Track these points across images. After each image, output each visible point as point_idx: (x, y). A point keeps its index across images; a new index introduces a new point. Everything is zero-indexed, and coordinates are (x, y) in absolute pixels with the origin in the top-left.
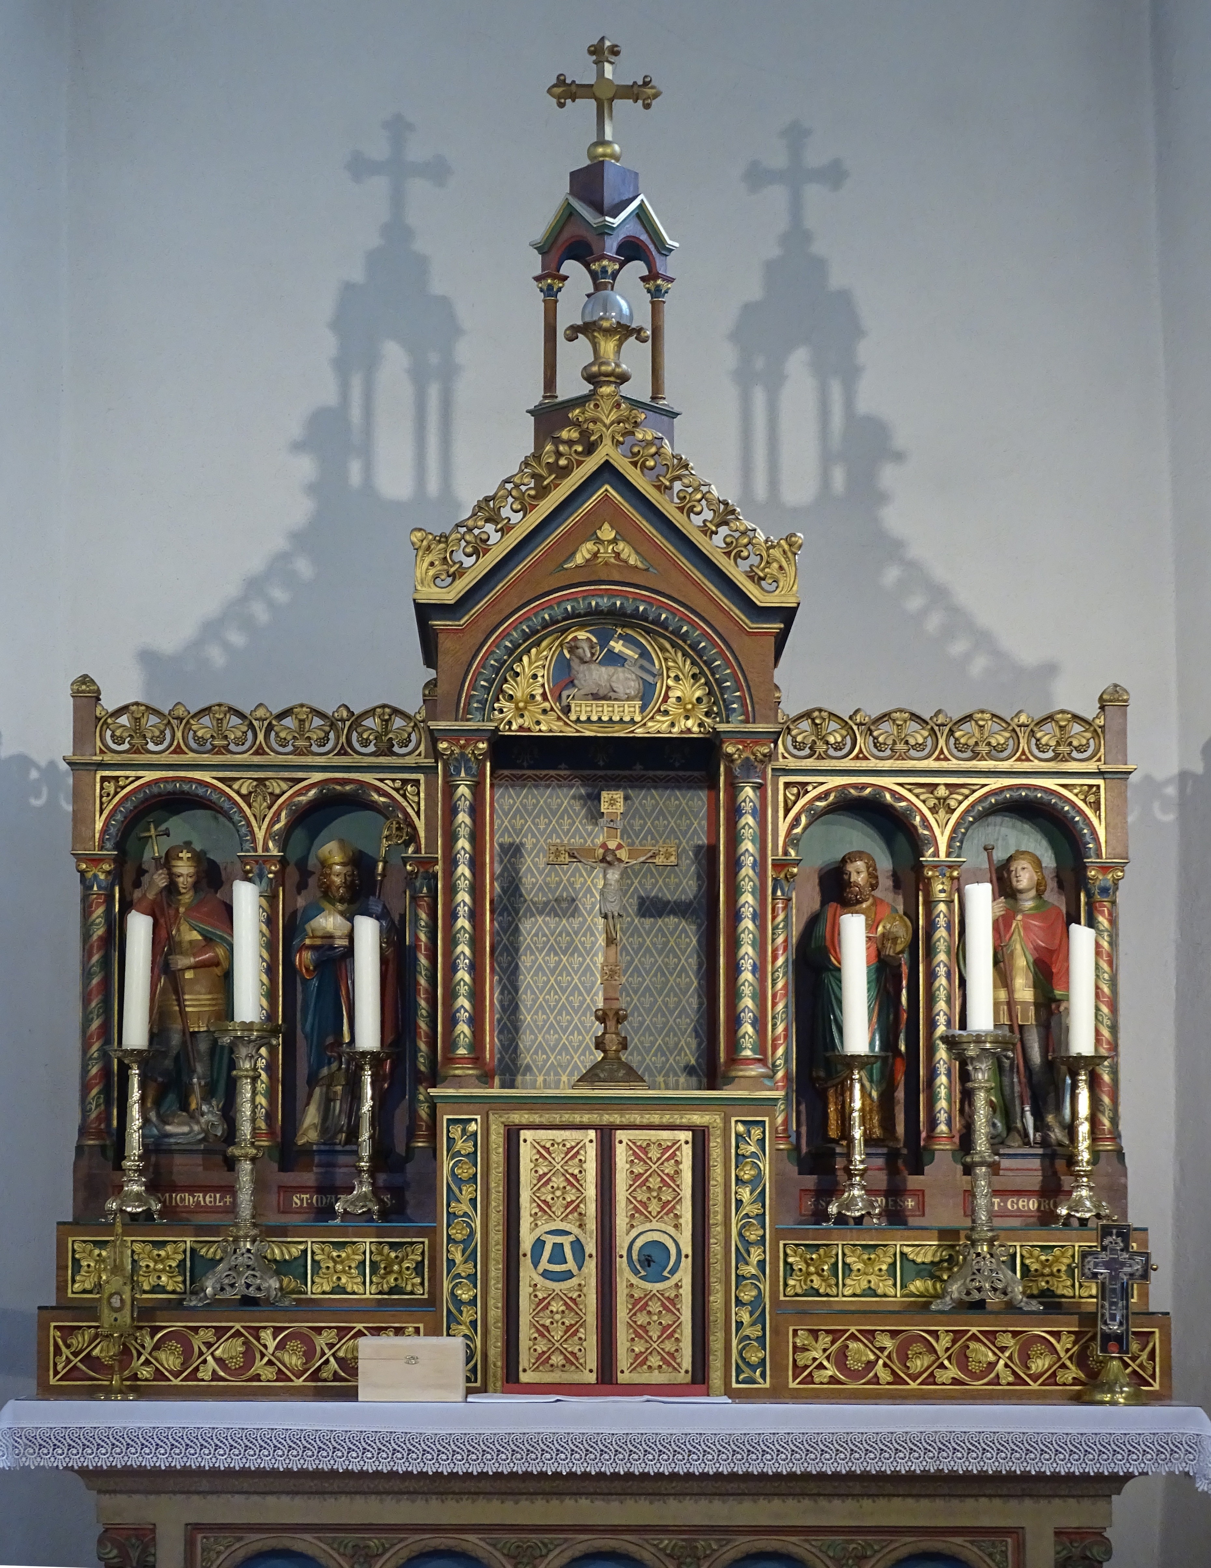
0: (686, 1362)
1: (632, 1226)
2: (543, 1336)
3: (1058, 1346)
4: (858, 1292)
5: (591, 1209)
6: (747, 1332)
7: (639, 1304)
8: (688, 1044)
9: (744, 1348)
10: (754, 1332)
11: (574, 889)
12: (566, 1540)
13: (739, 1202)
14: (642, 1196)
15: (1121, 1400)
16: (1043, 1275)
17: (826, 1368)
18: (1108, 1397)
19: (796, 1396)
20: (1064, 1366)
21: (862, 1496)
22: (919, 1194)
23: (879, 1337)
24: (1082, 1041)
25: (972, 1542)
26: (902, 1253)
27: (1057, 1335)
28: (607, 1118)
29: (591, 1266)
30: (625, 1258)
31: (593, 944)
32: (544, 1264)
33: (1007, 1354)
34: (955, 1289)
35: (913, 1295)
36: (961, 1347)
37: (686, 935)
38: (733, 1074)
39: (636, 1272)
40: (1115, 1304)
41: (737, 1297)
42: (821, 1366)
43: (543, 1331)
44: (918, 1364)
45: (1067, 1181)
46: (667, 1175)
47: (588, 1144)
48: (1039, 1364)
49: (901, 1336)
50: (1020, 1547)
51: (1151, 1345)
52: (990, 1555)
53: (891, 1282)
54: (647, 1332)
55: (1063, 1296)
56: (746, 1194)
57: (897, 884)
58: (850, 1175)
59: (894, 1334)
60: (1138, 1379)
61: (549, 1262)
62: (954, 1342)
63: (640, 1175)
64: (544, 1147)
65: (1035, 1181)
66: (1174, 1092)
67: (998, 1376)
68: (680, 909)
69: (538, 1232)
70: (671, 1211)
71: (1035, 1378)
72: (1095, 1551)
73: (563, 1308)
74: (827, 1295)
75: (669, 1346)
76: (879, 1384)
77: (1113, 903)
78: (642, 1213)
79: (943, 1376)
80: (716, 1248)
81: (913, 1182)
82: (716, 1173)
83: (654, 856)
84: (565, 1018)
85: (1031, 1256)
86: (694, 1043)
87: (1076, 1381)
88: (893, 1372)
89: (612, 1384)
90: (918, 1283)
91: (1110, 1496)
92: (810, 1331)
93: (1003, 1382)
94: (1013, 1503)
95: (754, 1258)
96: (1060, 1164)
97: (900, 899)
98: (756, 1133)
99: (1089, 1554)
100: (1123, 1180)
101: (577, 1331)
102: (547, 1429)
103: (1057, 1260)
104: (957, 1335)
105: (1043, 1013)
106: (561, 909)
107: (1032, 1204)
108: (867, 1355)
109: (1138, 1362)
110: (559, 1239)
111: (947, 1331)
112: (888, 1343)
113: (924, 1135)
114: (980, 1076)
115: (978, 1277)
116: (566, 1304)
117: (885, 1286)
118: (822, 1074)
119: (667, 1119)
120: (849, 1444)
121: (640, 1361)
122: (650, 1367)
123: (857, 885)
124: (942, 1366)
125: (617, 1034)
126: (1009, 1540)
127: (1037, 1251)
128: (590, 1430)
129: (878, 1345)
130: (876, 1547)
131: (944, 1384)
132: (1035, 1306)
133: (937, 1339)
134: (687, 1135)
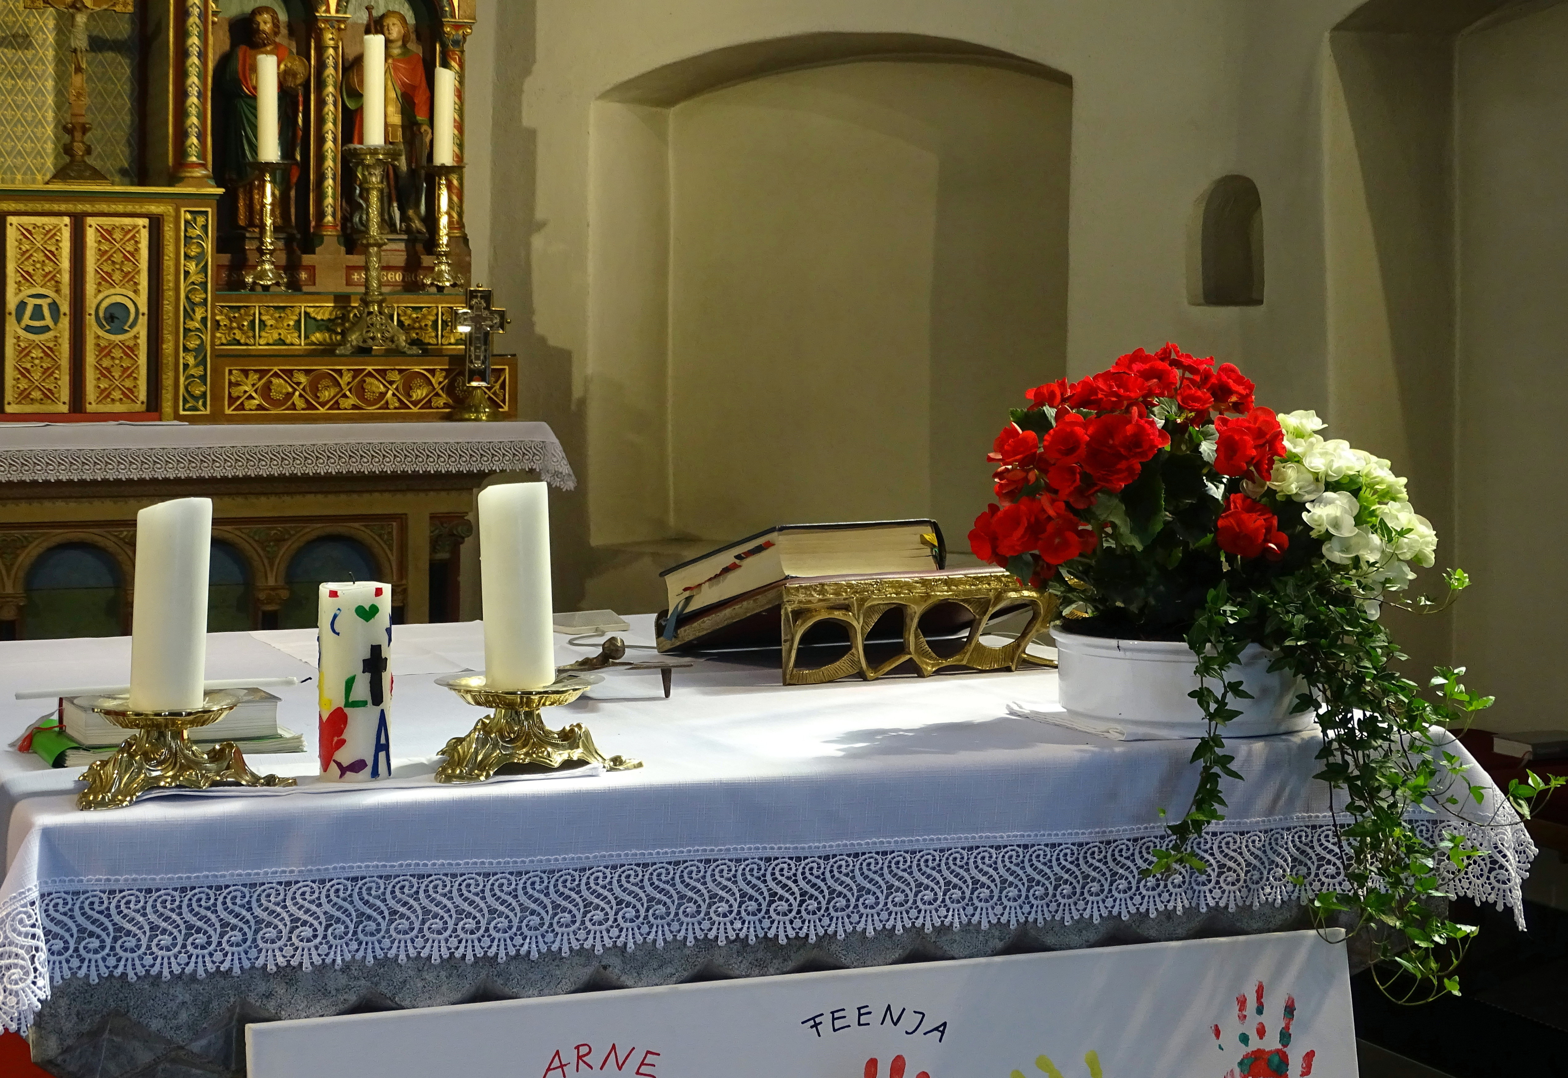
0: (142, 395)
1: (100, 291)
2: (26, 377)
3: (433, 381)
4: (271, 341)
5: (65, 278)
6: (192, 372)
7: (104, 351)
8: (122, 152)
9: (189, 384)
10: (198, 372)
11: (28, 28)
12: (43, 534)
13: (187, 273)
14: (107, 268)
16: (414, 328)
17: (253, 398)
19: (231, 420)
20: (437, 394)
21: (283, 493)
22: (311, 270)
23: (296, 375)
24: (444, 155)
25: (365, 526)
26: (306, 313)
27: (432, 372)
28: (80, 207)
29: (65, 323)
30: (93, 317)
31: (44, 71)
32: (26, 320)
34: (354, 338)
35: (314, 344)
36: (359, 382)
37: (121, 68)
38: (183, 175)
39: (102, 326)
40: (479, 348)
41: (184, 345)
42: (251, 397)
43: (24, 373)
44: (326, 395)
45: (427, 260)
46: (128, 252)
47: (63, 228)
48: (419, 393)
50: (403, 529)
52: (380, 536)
53: (296, 335)
54: (110, 372)
55: (429, 344)
56: (192, 267)
57: (292, 32)
58: (262, 253)
59: (307, 372)
60: (494, 405)
61: (31, 319)
62: (354, 378)
63: (106, 252)
64: (27, 230)
65: (400, 259)
66: (489, 194)
67: (387, 403)
68: (116, 46)
69: (21, 296)
70: (131, 279)
71: (415, 404)
72: (459, 529)
73: (42, 355)
74: (247, 344)
75: (128, 383)
77: (462, 52)
78: (107, 281)
79: (344, 403)
80: (168, 307)
81: (307, 259)
82: (169, 249)
83: (114, 5)
84: (20, 128)
85: (405, 314)
86: (127, 151)
87: (446, 405)
88: (307, 401)
89: (81, 412)
90: (318, 335)
92: (242, 370)
93: (391, 407)
94: (399, 496)
95: (199, 315)
96: (419, 247)
97: (294, 44)
98: (201, 220)
100: (467, 259)
101: (53, 372)
102: (37, 447)
103: (424, 317)
105: (408, 133)
106: (17, 43)
107: (398, 277)
110: (38, 301)
112: (303, 379)
113: (313, 224)
114: (374, 179)
115: (373, 329)
116: (44, 351)
117: (291, 337)
118: (234, 177)
119: (130, 208)
120: (279, 454)
121: (104, 395)
122: (113, 400)
123: (264, 32)
124: (345, 396)
125: (83, 142)
127: (409, 311)
128: (73, 447)
129: (295, 380)
132: (416, 350)
133: (341, 375)
134: (145, 221)
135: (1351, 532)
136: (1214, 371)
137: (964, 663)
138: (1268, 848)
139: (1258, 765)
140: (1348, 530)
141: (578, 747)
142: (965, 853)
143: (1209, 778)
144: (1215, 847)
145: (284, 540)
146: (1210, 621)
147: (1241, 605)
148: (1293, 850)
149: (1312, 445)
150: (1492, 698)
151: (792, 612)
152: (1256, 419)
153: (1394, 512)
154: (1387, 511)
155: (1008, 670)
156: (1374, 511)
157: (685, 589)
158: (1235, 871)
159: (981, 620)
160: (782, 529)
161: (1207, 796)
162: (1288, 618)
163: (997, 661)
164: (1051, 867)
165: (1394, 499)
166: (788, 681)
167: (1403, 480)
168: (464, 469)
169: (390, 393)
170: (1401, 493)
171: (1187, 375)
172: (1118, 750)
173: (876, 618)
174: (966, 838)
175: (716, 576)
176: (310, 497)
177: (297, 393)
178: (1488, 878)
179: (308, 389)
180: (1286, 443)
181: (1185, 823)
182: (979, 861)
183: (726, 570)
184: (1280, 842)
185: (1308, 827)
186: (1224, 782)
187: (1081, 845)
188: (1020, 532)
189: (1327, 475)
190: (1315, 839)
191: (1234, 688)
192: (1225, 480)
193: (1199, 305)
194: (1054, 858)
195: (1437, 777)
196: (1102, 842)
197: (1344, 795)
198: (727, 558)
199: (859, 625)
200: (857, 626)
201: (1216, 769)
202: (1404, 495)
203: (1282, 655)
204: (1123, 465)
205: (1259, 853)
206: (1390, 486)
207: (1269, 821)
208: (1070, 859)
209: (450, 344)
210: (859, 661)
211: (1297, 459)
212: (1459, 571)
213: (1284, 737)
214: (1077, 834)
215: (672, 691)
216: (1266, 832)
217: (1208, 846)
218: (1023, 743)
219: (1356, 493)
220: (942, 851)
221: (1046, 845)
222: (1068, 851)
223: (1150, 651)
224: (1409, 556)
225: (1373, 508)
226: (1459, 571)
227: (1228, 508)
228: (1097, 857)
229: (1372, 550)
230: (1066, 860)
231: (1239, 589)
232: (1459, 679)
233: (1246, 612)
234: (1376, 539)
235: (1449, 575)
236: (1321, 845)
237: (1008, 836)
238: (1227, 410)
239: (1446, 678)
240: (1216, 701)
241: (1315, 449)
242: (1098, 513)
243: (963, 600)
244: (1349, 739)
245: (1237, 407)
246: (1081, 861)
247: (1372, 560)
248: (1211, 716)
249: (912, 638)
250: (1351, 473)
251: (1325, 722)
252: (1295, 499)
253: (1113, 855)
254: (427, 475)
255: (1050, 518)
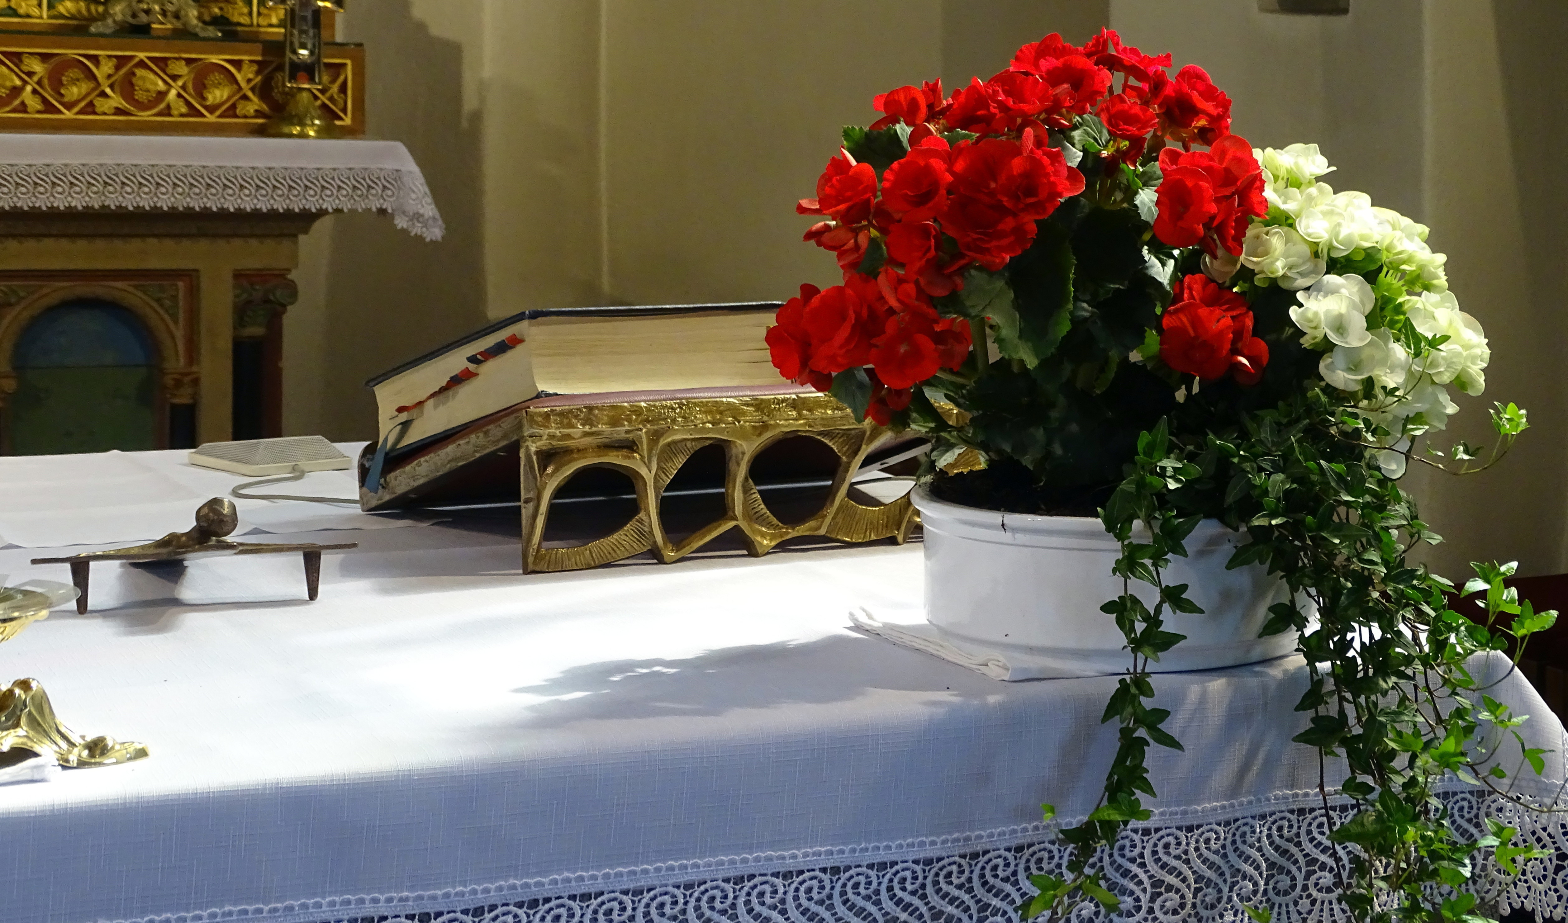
3: (239, 77)
15: (312, 133)
18: (296, 130)
20: (245, 98)
23: (26, 60)
25: (136, 287)
27: (238, 64)
33: (180, 83)
35: (61, 16)
48: (218, 94)
49: (54, 60)
50: (194, 291)
51: (342, 78)
52: (158, 300)
59: (45, 57)
60: (329, 114)
62: (118, 68)
71: (211, 109)
72: (278, 293)
76: (25, 112)
79: (101, 105)
87: (259, 114)
88: (45, 101)
91: (295, 236)
93: (175, 112)
94: (186, 243)
99: (272, 297)
104: (121, 61)
108: (12, 80)
109: (328, 95)
111: (109, 57)
112: (38, 67)
124: (103, 94)
126: (181, 284)
130: (22, 294)
131: (105, 114)
132: (213, 32)
135: (1361, 340)
136: (1171, 75)
137: (822, 532)
138: (1230, 848)
139: (1216, 714)
140: (1357, 336)
141: (17, 725)
142: (729, 887)
143: (1131, 748)
144: (1147, 853)
145: (10, 305)
146: (1141, 484)
147: (1191, 458)
148: (1269, 850)
149: (1310, 199)
150: (1554, 613)
151: (537, 453)
152: (1223, 152)
153: (1430, 308)
154: (1419, 305)
155: (892, 541)
156: (1401, 305)
157: (401, 410)
158: (1178, 891)
159: (849, 464)
160: (535, 315)
161: (1126, 778)
162: (1259, 480)
163: (874, 527)
164: (878, 903)
165: (1427, 288)
166: (531, 567)
167: (1441, 258)
168: (280, 205)
169: (173, 93)
170: (1437, 278)
171: (1132, 81)
172: (993, 699)
173: (679, 462)
174: (733, 862)
175: (443, 390)
176: (49, 243)
177: (29, 88)
178: (1554, 882)
179: (46, 82)
180: (1269, 193)
181: (1090, 824)
182: (755, 901)
183: (456, 381)
184: (1250, 839)
185: (1292, 812)
186: (1154, 754)
187: (928, 862)
188: (844, 333)
189: (1331, 248)
190: (1303, 831)
191: (1174, 596)
192: (1176, 252)
193: (1272, 11)
194: (883, 888)
195: (1476, 736)
196: (963, 856)
197: (1339, 764)
198: (455, 361)
199: (652, 475)
200: (648, 474)
201: (1142, 732)
202: (1442, 280)
203: (1250, 540)
204: (1009, 223)
205: (1216, 859)
206: (1421, 267)
207: (1232, 806)
208: (909, 887)
209: (271, 26)
210: (651, 532)
211: (1286, 221)
212: (1512, 405)
213: (1257, 669)
214: (922, 844)
215: (321, 588)
216: (1227, 823)
217: (1137, 851)
218: (845, 690)
219: (1371, 277)
220: (689, 886)
221: (871, 866)
222: (908, 874)
223: (1050, 532)
224: (1447, 378)
225: (1400, 300)
226: (1512, 405)
227: (1178, 298)
228: (956, 881)
229: (1393, 369)
230: (904, 889)
231: (1189, 429)
232: (1508, 582)
233: (1196, 470)
234: (1399, 352)
235: (1498, 413)
236: (1312, 840)
237: (806, 855)
238: (1193, 139)
239: (1488, 581)
240: (1147, 618)
241: (1313, 206)
242: (968, 303)
243: (820, 433)
244: (1346, 676)
245: (1204, 136)
246: (930, 890)
247: (1391, 385)
248: (1137, 644)
249: (741, 494)
250: (1367, 245)
251: (1312, 649)
252: (1284, 285)
253: (982, 876)
254: (223, 215)
255: (891, 311)
